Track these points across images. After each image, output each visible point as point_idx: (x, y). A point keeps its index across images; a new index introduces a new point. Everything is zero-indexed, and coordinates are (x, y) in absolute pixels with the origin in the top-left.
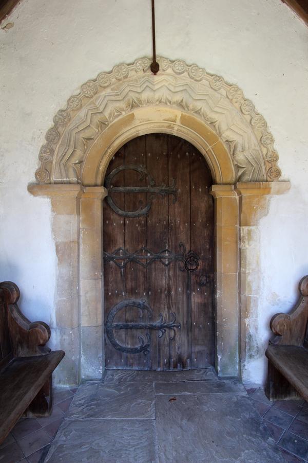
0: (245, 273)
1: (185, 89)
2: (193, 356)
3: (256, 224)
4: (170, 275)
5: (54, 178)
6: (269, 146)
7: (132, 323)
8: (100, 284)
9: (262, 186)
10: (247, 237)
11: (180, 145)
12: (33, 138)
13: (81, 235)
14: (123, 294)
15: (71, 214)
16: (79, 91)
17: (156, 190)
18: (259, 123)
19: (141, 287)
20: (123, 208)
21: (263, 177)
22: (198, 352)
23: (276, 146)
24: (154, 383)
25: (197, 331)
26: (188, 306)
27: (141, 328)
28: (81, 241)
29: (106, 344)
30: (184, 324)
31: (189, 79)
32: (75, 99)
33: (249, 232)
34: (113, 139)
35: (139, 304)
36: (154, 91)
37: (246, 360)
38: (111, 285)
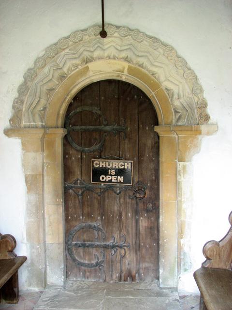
0: (181, 201)
1: (129, 48)
2: (141, 271)
3: (190, 160)
4: (121, 202)
5: (24, 123)
6: (199, 95)
7: (89, 243)
8: (61, 210)
9: (193, 129)
10: (182, 171)
11: (129, 89)
12: (8, 91)
13: (45, 168)
14: (81, 218)
15: (36, 151)
16: (43, 53)
17: (108, 128)
18: (191, 76)
19: (96, 212)
20: (80, 144)
21: (197, 120)
22: (145, 268)
23: (207, 96)
24: (105, 290)
25: (144, 251)
26: (136, 229)
27: (97, 246)
28: (45, 173)
29: (67, 259)
30: (133, 244)
31: (132, 40)
32: (41, 59)
33: (184, 167)
34: (71, 88)
35: (95, 227)
36: (104, 50)
37: (182, 273)
38: (70, 210)
